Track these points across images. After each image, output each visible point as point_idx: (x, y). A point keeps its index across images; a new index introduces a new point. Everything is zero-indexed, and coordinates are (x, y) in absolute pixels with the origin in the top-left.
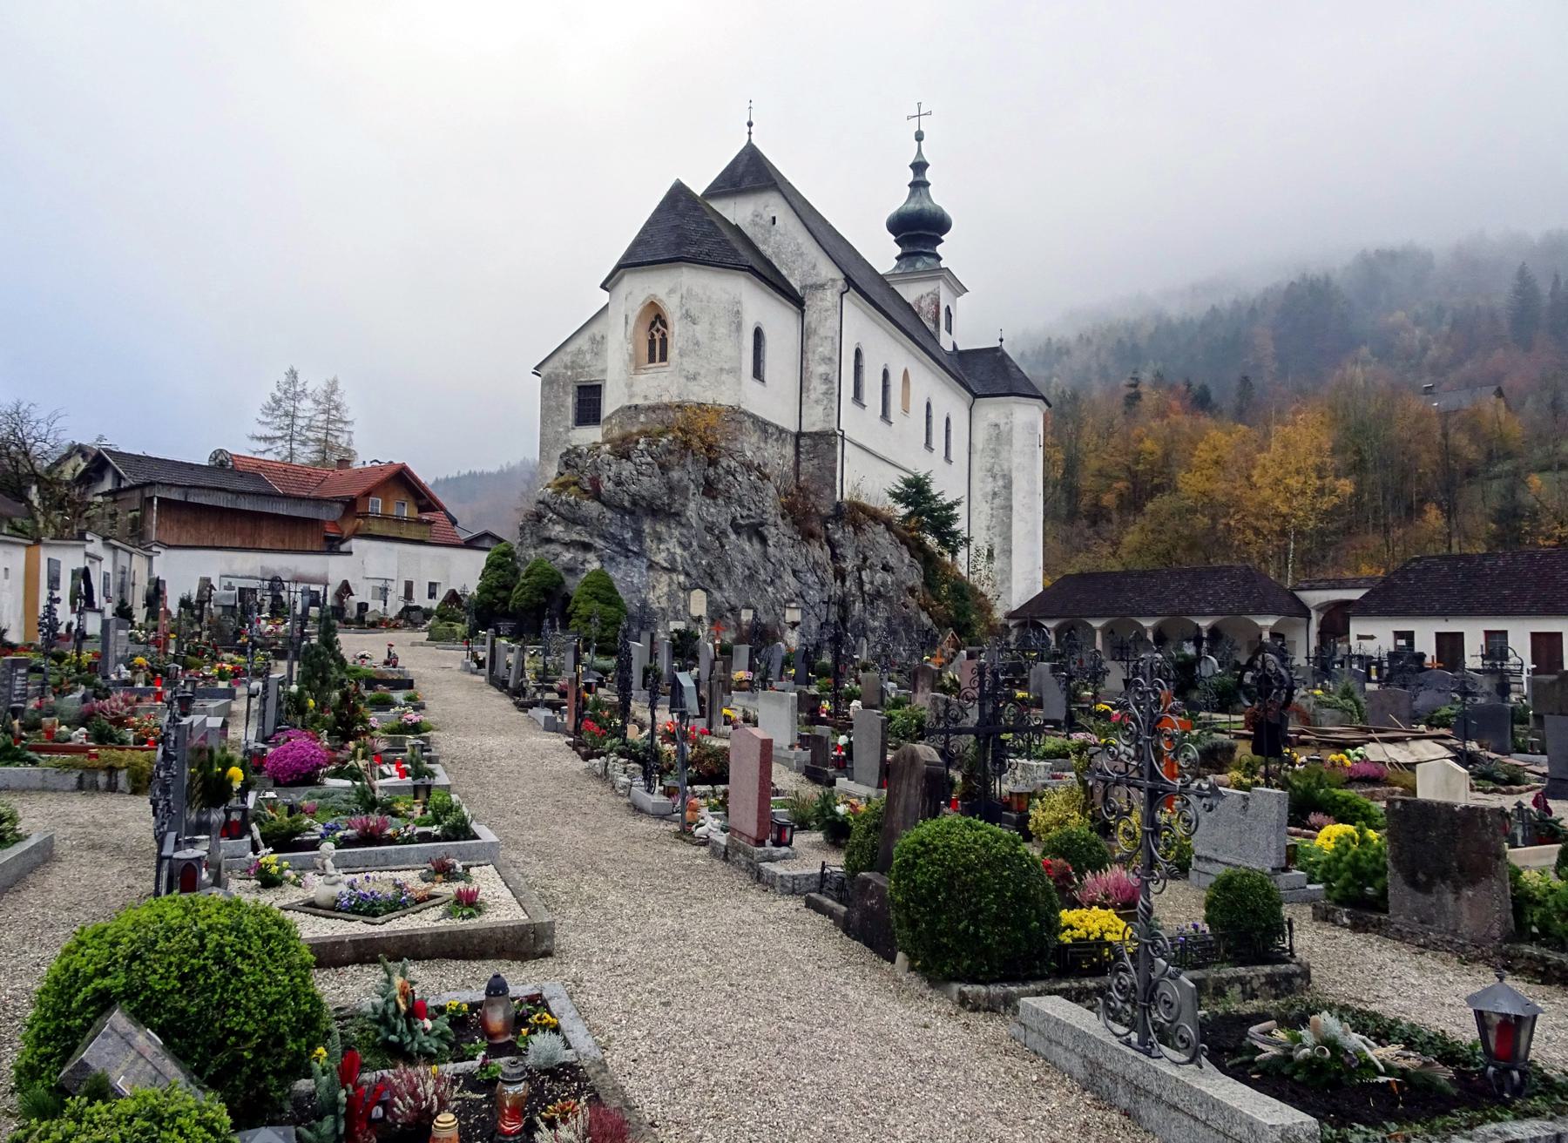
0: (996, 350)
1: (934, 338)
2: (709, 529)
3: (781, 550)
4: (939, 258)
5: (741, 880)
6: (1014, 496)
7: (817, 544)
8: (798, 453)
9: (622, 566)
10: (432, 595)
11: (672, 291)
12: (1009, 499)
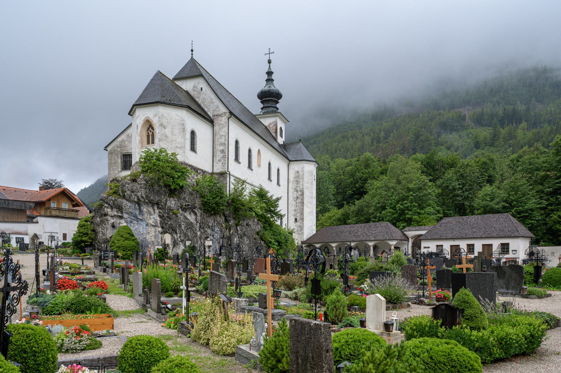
1: (275, 139)
4: (278, 109)
6: (305, 198)
11: (155, 115)
12: (303, 200)
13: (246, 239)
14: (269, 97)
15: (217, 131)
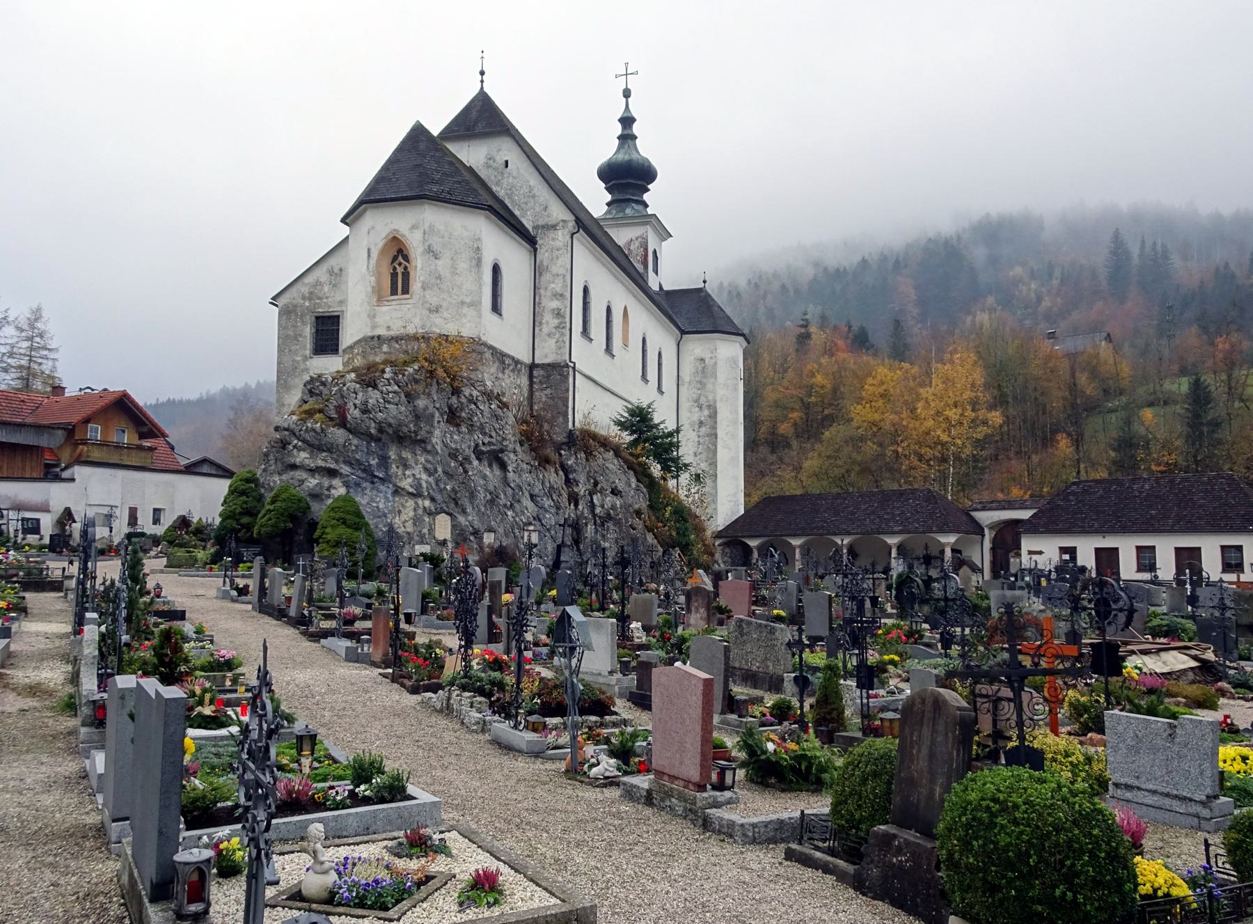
0: (699, 290)
2: (453, 455)
3: (520, 476)
4: (646, 206)
5: (691, 832)
6: (719, 425)
7: (553, 470)
8: (531, 383)
9: (368, 492)
10: (156, 521)
11: (414, 227)
13: (612, 527)
14: (626, 178)
15: (545, 264)
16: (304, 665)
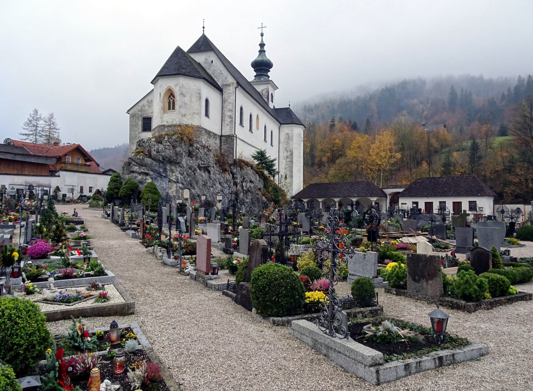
1: (267, 104)
2: (190, 168)
3: (215, 176)
4: (269, 77)
5: (201, 286)
6: (294, 158)
7: (228, 174)
8: (221, 142)
9: (159, 181)
10: (90, 191)
11: (176, 85)
12: (292, 159)
15: (226, 98)
16: (114, 239)
